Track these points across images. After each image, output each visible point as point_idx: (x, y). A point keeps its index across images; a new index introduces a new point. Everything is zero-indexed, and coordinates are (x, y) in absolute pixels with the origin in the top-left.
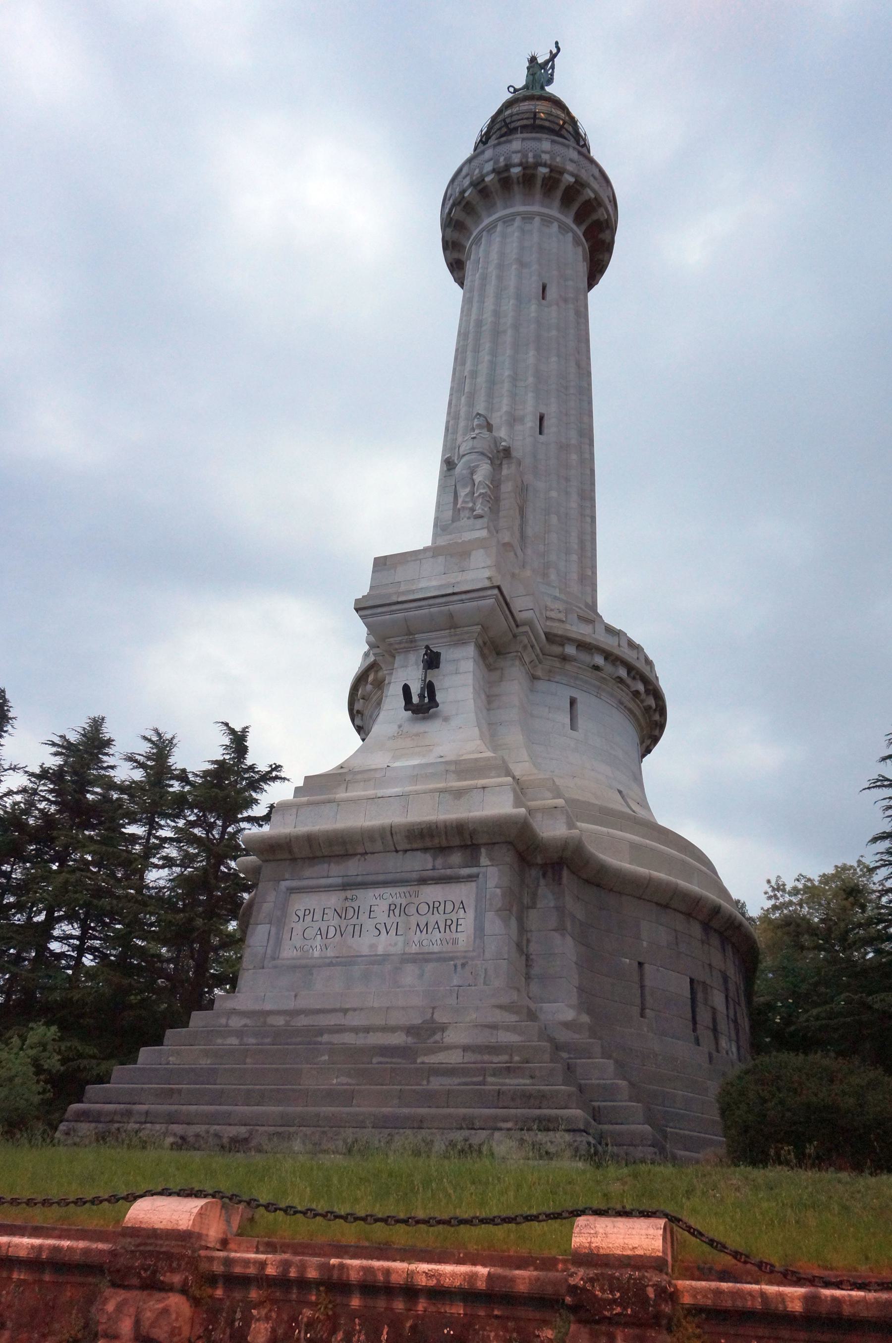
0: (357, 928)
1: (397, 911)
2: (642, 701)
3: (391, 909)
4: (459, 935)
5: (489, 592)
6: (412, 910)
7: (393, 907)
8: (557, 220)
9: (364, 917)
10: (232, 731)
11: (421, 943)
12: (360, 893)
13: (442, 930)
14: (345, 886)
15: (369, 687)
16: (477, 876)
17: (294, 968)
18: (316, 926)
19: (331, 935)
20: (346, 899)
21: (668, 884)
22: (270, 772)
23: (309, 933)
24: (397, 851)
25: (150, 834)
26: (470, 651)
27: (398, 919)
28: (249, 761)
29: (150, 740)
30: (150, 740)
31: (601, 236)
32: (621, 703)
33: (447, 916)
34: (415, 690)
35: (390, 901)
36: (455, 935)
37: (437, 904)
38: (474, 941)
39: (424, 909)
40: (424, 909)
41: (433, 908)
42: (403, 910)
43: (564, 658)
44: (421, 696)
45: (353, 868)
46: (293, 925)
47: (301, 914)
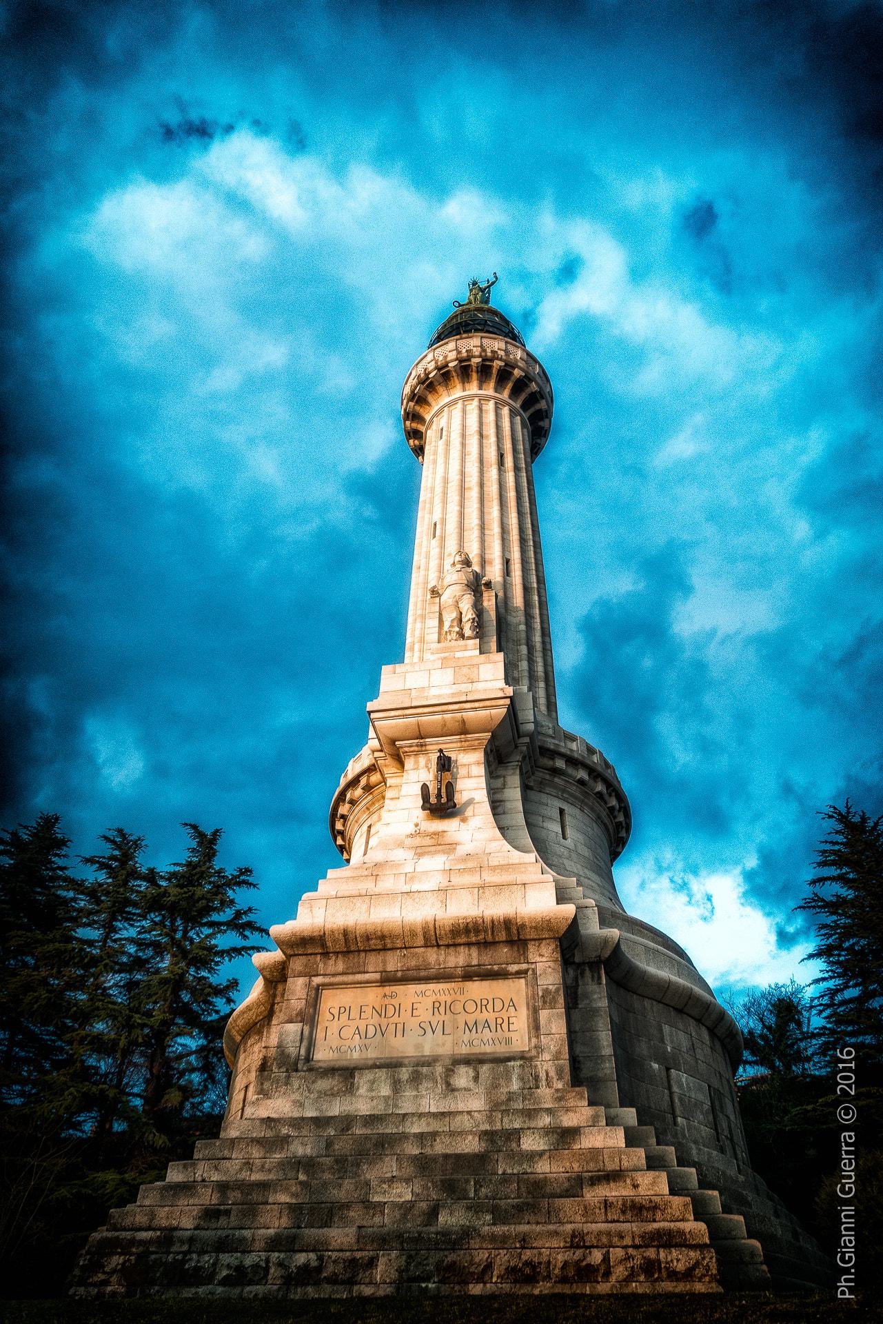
0: (400, 1027)
1: (442, 1009)
2: (615, 817)
3: (436, 1007)
4: (511, 1034)
5: (502, 702)
6: (458, 1007)
7: (437, 1005)
8: (509, 404)
9: (406, 1015)
10: (201, 835)
11: (471, 1043)
12: (399, 989)
13: (493, 1028)
14: (388, 979)
15: (358, 792)
16: (526, 972)
17: (331, 1071)
18: (353, 1025)
19: (370, 1034)
20: (385, 996)
21: (684, 988)
22: (238, 876)
23: (347, 1033)
24: (438, 946)
25: (107, 937)
26: (479, 756)
27: (442, 1018)
28: (217, 864)
29: (113, 842)
30: (113, 842)
31: (541, 424)
32: (599, 817)
33: (497, 1015)
34: (433, 790)
35: (434, 998)
36: (507, 1034)
37: (485, 1002)
38: (530, 1039)
39: (471, 1007)
40: (471, 1007)
41: (482, 1005)
42: (449, 1008)
43: (555, 771)
44: (439, 796)
45: (393, 963)
46: (327, 1024)
47: (335, 1012)
